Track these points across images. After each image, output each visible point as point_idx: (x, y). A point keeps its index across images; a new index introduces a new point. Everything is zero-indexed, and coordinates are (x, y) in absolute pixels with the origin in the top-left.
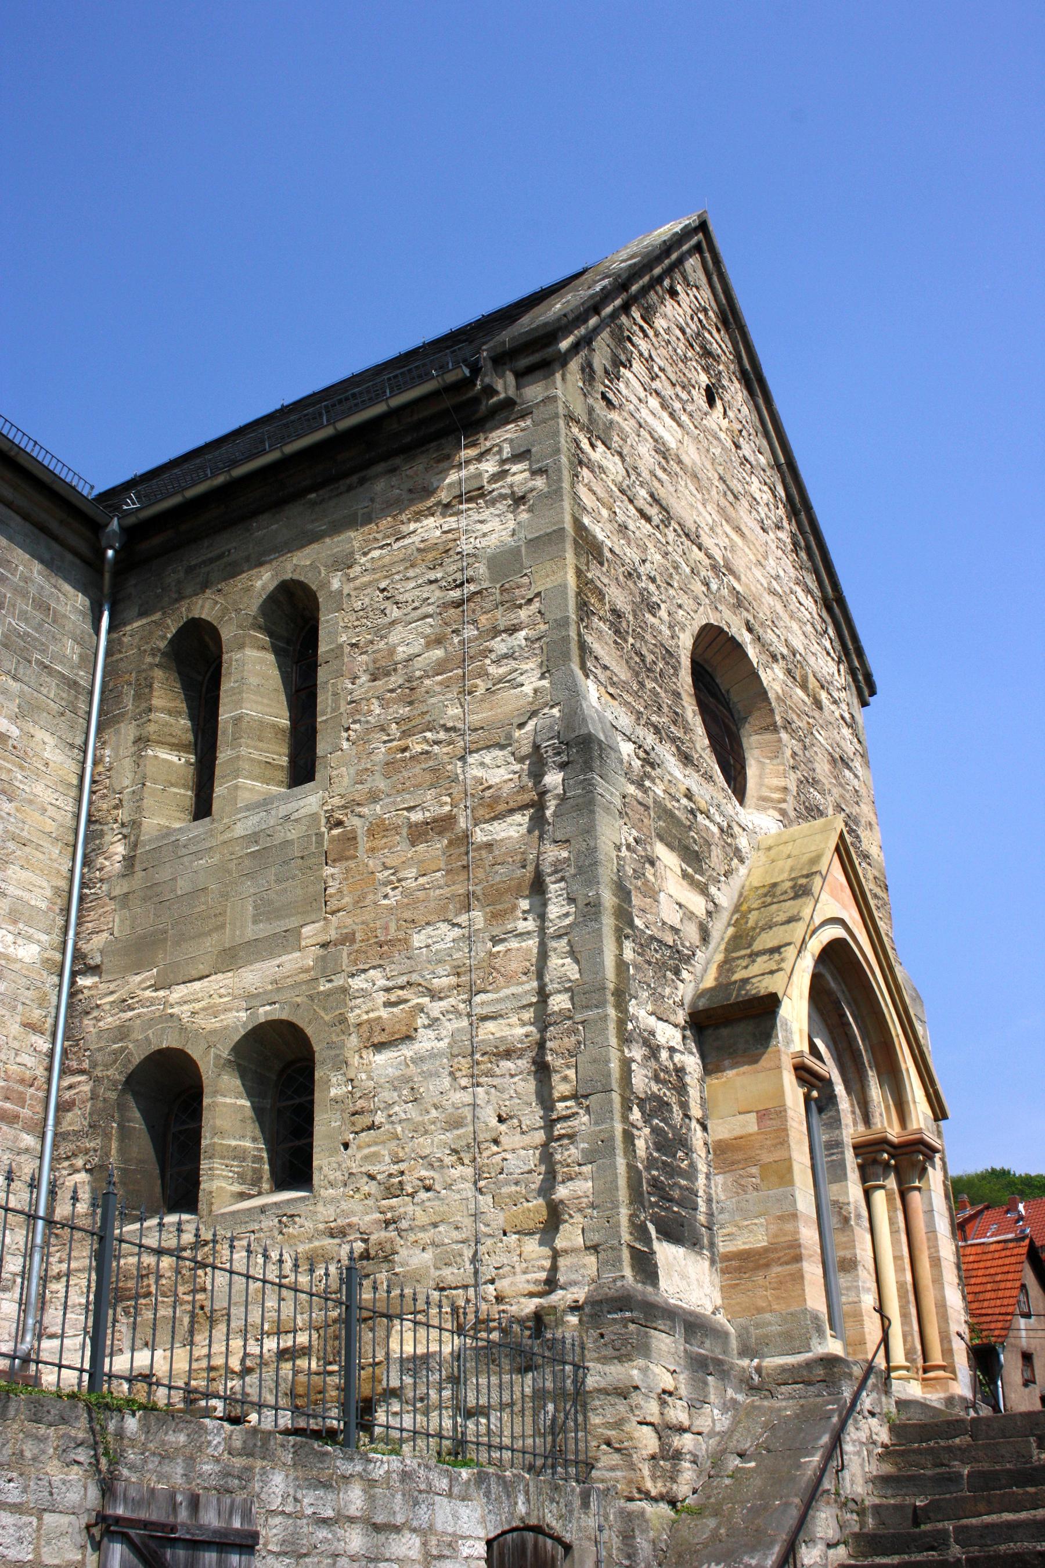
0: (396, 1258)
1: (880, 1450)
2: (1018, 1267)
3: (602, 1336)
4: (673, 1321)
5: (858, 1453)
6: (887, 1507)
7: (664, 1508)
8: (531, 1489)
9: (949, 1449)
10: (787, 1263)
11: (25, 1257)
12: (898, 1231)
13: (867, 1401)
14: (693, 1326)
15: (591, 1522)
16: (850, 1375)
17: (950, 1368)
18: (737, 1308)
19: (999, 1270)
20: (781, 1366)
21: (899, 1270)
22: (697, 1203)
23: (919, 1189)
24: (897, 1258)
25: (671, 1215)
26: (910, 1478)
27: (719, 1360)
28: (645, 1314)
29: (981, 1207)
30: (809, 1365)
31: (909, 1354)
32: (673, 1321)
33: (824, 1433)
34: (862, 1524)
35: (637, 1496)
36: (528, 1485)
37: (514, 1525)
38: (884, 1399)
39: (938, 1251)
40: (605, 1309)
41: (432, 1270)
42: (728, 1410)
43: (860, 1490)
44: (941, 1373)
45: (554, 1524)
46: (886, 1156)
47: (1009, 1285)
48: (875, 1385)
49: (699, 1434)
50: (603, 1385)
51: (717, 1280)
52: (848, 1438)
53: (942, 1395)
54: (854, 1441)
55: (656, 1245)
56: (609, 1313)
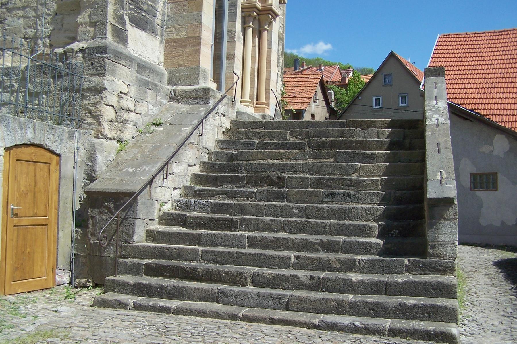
0: (6, 22)
1: (224, 130)
2: (316, 85)
3: (92, 64)
4: (131, 62)
5: (213, 130)
6: (221, 153)
7: (115, 143)
8: (37, 127)
9: (253, 133)
10: (194, 46)
11: (353, 157)
12: (255, 47)
13: (221, 109)
14: (143, 67)
15: (72, 145)
16: (215, 97)
17: (268, 104)
18: (170, 64)
19: (309, 85)
20: (185, 90)
21: (253, 62)
22: (156, 14)
23: (267, 30)
24: (253, 58)
25: (140, 16)
26: (233, 142)
27: (155, 84)
28: (115, 56)
29: (309, 66)
30: (197, 90)
31: (251, 97)
32: (131, 62)
33: (196, 119)
34: (209, 159)
35: (100, 136)
36: (35, 125)
37: (24, 142)
38: (230, 109)
39: (271, 57)
40: (95, 52)
41: (22, 29)
42: (157, 106)
43: (211, 145)
44: (263, 106)
45: (50, 144)
46: (255, 13)
47: (311, 91)
48: (227, 104)
49: (140, 114)
50: (90, 86)
51: (163, 50)
52: (208, 123)
53: (261, 114)
54: (211, 125)
55: (129, 27)
56: (97, 53)
